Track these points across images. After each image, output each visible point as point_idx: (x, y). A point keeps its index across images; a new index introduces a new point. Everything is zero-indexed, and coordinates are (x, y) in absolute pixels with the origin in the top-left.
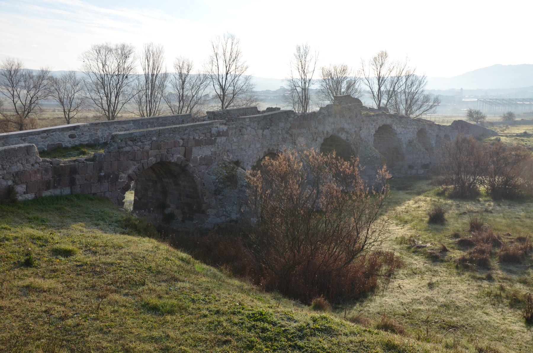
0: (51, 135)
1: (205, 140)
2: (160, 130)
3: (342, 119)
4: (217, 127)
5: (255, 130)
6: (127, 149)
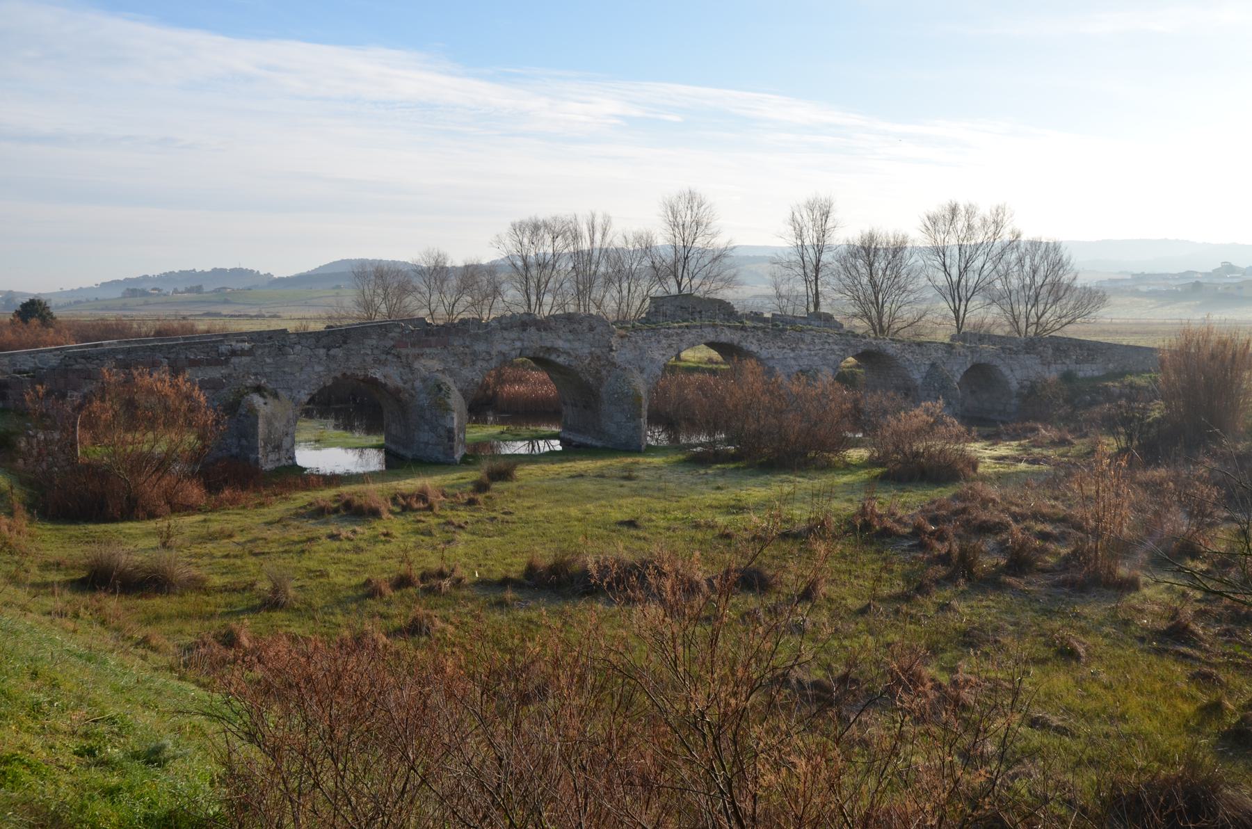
3: (543, 334)
4: (231, 345)
5: (311, 349)
6: (77, 366)
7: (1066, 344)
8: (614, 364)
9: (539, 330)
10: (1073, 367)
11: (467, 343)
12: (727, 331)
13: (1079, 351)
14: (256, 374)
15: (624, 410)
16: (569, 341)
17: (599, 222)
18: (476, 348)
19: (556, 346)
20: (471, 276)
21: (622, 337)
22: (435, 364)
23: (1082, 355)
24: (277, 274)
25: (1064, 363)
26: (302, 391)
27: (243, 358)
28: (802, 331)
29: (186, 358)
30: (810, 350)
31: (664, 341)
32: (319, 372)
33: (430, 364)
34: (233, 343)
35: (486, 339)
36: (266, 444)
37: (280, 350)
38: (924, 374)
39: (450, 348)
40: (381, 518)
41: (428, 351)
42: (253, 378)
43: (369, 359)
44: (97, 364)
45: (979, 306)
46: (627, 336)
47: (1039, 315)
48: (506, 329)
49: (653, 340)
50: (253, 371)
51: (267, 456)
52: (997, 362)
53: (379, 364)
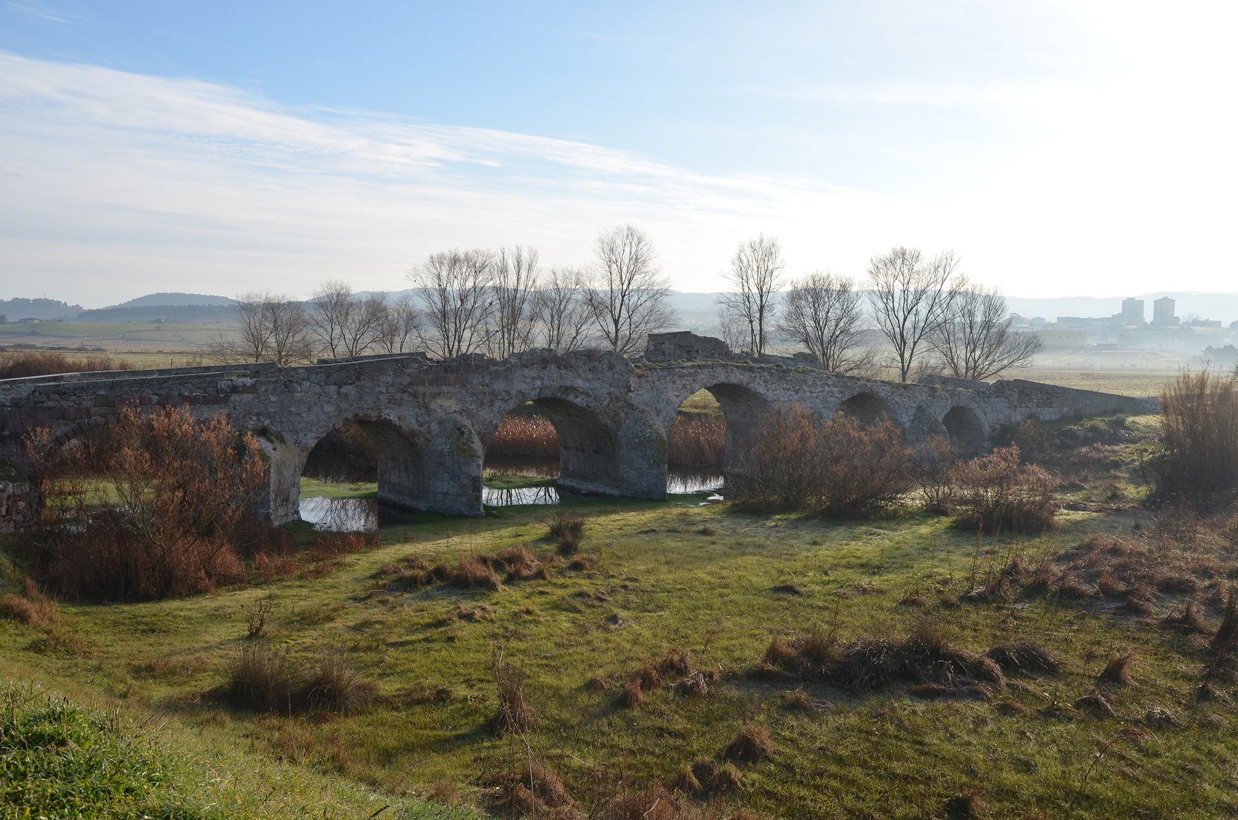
0: (18, 387)
1: (203, 397)
2: (112, 382)
3: (564, 372)
4: (231, 380)
5: (321, 386)
6: (50, 404)
7: (1029, 388)
8: (631, 406)
9: (559, 368)
10: (1034, 410)
11: (487, 381)
12: (737, 373)
13: (1040, 395)
14: (258, 415)
15: (645, 455)
16: (588, 380)
17: (525, 256)
18: (496, 387)
19: (575, 386)
20: (375, 309)
21: (639, 377)
22: (452, 405)
23: (1042, 399)
24: (87, 306)
25: (1027, 407)
26: (309, 435)
27: (245, 396)
28: (804, 372)
29: (180, 395)
30: (811, 392)
31: (678, 382)
32: (329, 413)
33: (447, 405)
34: (234, 378)
35: (506, 377)
36: (276, 498)
37: (286, 386)
38: (912, 418)
39: (469, 387)
40: (497, 590)
41: (445, 389)
42: (254, 418)
43: (383, 398)
44: (73, 401)
45: (924, 349)
46: (644, 375)
47: (976, 359)
48: (526, 366)
49: (668, 380)
50: (255, 410)
51: (277, 510)
52: (973, 406)
53: (394, 404)
